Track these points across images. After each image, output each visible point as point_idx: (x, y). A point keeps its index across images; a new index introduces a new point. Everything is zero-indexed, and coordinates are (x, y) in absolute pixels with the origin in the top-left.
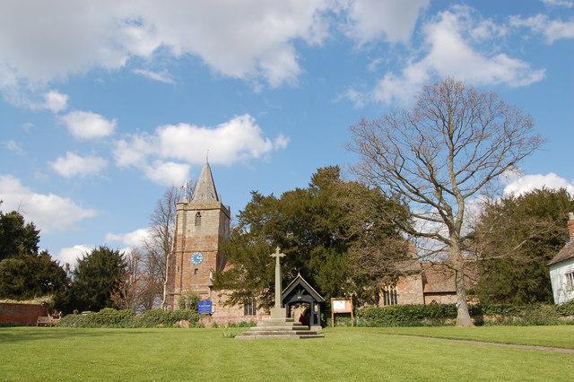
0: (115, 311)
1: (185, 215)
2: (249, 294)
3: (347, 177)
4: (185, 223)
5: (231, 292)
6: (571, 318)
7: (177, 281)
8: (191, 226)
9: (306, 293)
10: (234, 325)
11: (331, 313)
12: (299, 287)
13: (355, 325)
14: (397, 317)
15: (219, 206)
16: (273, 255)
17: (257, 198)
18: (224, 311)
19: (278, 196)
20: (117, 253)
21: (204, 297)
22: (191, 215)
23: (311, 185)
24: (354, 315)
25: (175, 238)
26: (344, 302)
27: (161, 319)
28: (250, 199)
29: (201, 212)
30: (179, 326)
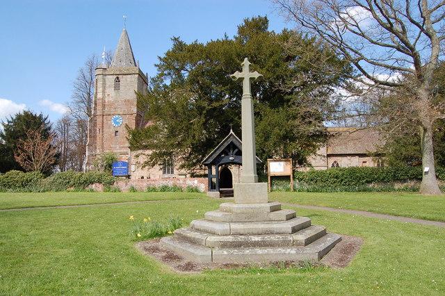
0: (21, 174)
1: (104, 80)
2: (170, 154)
3: (276, 26)
4: (104, 88)
5: (150, 152)
7: (98, 141)
8: (111, 91)
10: (154, 190)
11: (267, 176)
13: (295, 190)
14: (342, 180)
15: (137, 72)
16: (237, 75)
17: (179, 46)
18: (144, 174)
19: (233, 34)
20: (41, 116)
21: (124, 158)
22: (111, 80)
23: (236, 38)
24: (294, 178)
25: (95, 101)
26: (282, 163)
27: (72, 183)
28: (170, 46)
29: (120, 76)
30: (92, 191)
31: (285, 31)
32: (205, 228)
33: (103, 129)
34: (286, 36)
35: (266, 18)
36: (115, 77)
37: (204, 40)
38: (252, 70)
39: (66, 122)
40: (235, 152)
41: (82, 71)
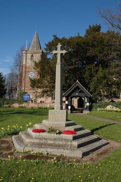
1: (26, 56)
3: (104, 30)
6: (4, 145)
7: (23, 85)
9: (81, 92)
12: (78, 88)
19: (83, 34)
25: (22, 66)
31: (108, 31)
32: (65, 138)
33: (25, 78)
34: (109, 32)
35: (100, 25)
36: (31, 54)
37: (67, 37)
38: (61, 50)
39: (12, 75)
40: (79, 91)
41: (18, 52)
